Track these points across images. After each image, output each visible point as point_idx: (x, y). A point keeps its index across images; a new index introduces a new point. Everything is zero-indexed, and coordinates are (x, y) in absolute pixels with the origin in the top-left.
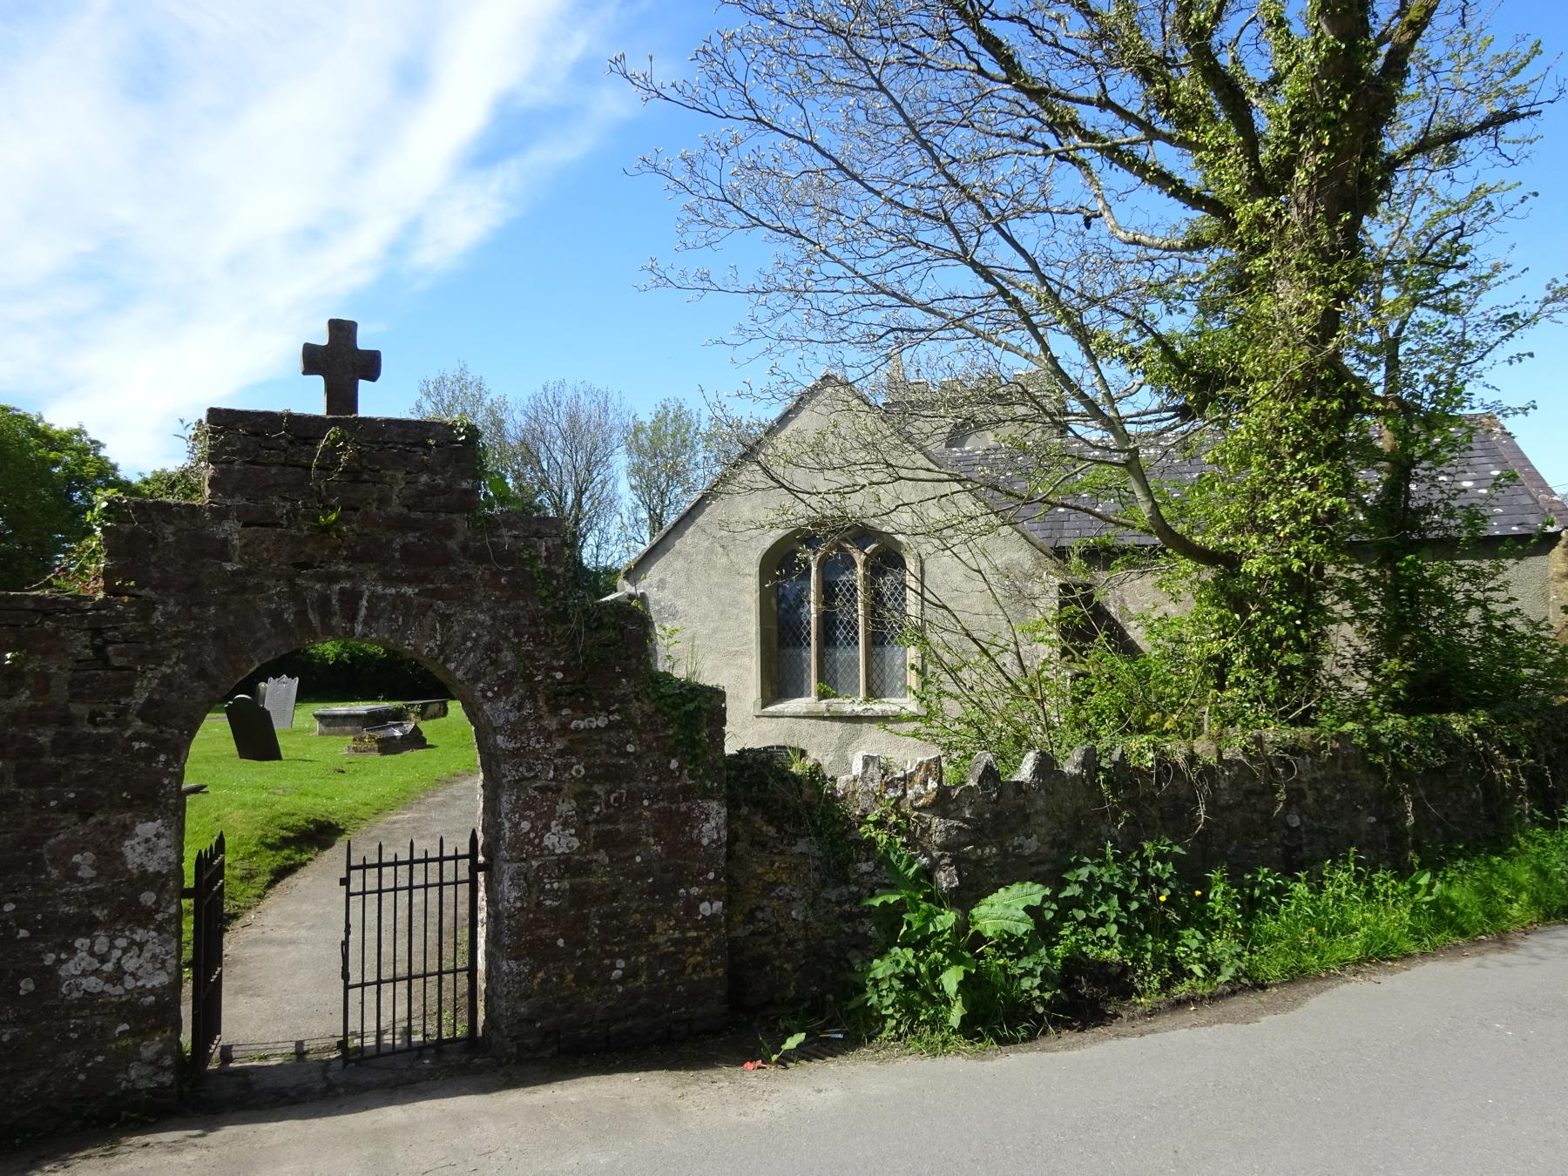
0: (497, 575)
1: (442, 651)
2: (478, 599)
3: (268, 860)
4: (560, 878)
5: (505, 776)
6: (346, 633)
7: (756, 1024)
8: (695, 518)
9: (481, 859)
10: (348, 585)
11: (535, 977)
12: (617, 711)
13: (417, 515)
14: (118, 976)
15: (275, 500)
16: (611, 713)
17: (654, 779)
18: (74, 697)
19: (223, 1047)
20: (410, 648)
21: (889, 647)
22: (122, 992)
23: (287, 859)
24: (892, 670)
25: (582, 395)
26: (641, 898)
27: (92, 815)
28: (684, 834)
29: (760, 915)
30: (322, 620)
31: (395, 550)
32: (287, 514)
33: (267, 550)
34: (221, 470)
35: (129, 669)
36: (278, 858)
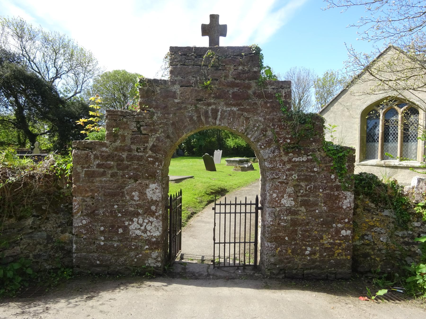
0: (266, 103)
1: (246, 131)
2: (259, 112)
3: (206, 198)
4: (287, 215)
5: (268, 177)
6: (213, 124)
7: (363, 279)
8: (338, 100)
9: (260, 205)
10: (214, 107)
11: (277, 249)
12: (311, 155)
13: (237, 81)
14: (145, 231)
15: (190, 77)
16: (308, 156)
17: (325, 182)
18: (132, 143)
19: (181, 254)
20: (235, 129)
21: (410, 143)
22: (146, 236)
23: (212, 198)
24: (411, 151)
25: (301, 70)
26: (318, 226)
27: (137, 180)
28: (336, 203)
29: (366, 237)
30: (206, 119)
31: (230, 94)
32: (194, 82)
33: (188, 95)
34: (174, 68)
35: (147, 135)
36: (209, 197)
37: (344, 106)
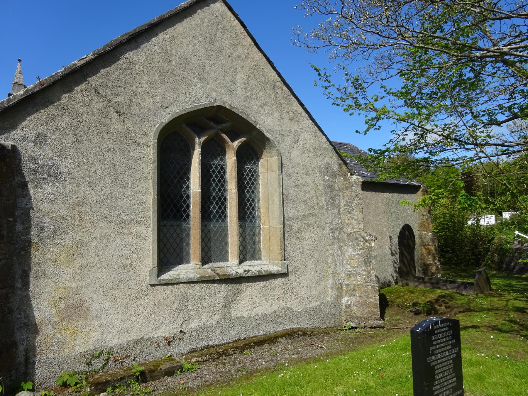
37: (109, 101)
